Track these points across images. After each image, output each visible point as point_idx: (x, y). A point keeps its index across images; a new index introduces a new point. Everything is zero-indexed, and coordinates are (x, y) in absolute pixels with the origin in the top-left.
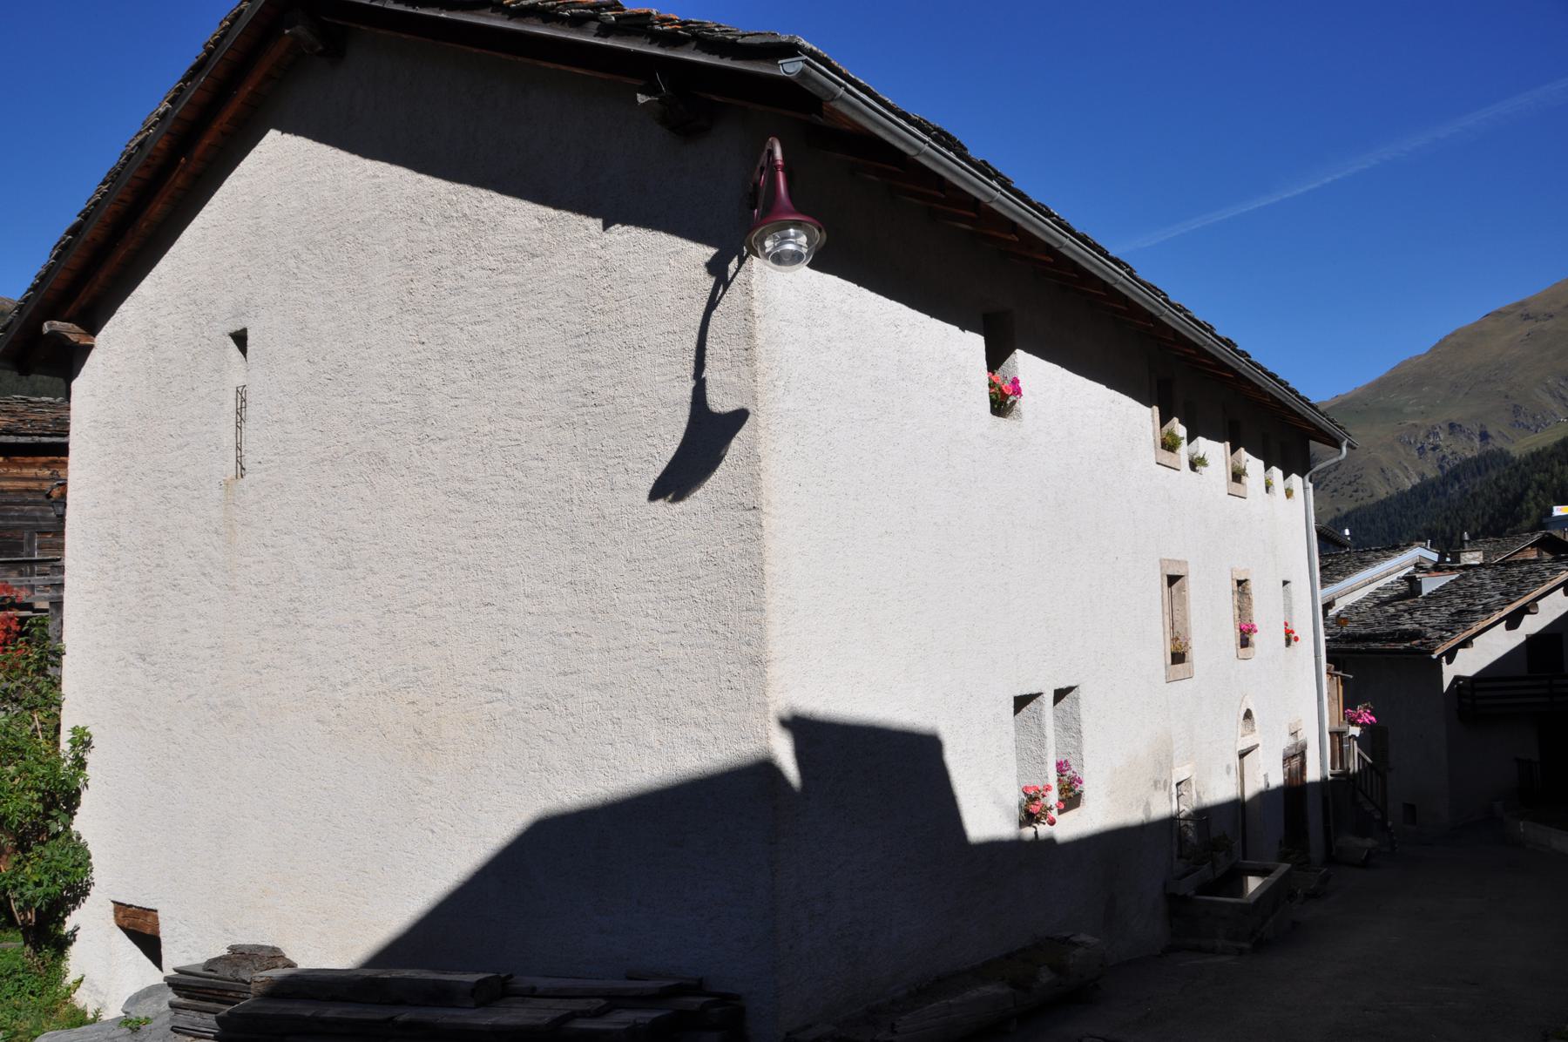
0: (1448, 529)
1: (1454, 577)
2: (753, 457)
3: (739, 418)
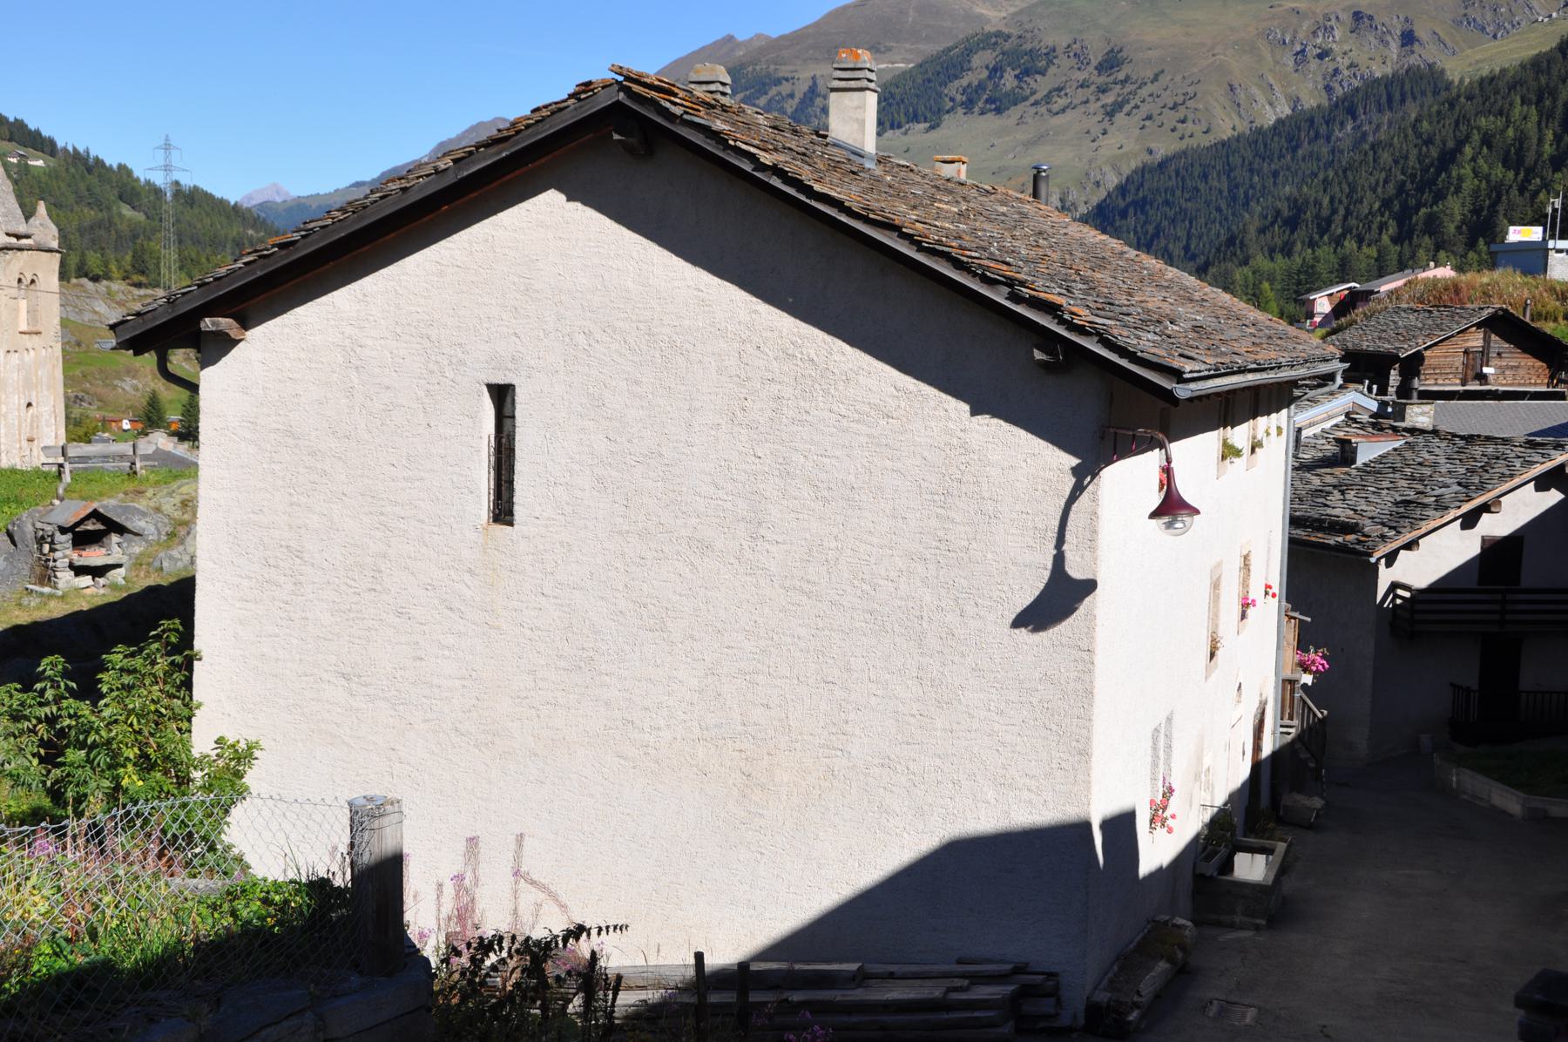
0: (1326, 201)
1: (1397, 444)
2: (1091, 617)
3: (1089, 586)
